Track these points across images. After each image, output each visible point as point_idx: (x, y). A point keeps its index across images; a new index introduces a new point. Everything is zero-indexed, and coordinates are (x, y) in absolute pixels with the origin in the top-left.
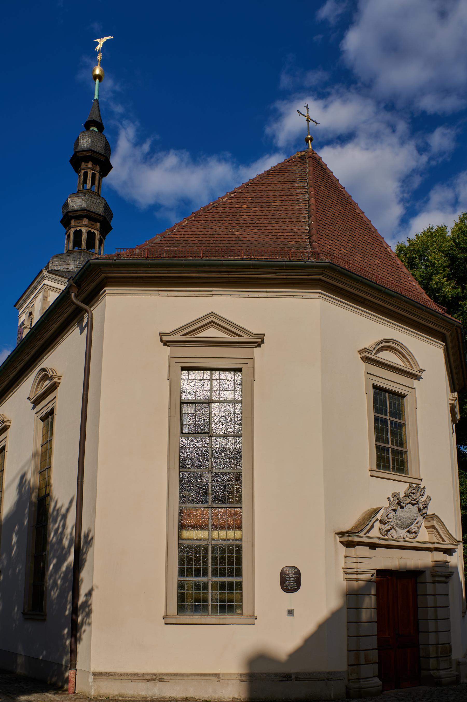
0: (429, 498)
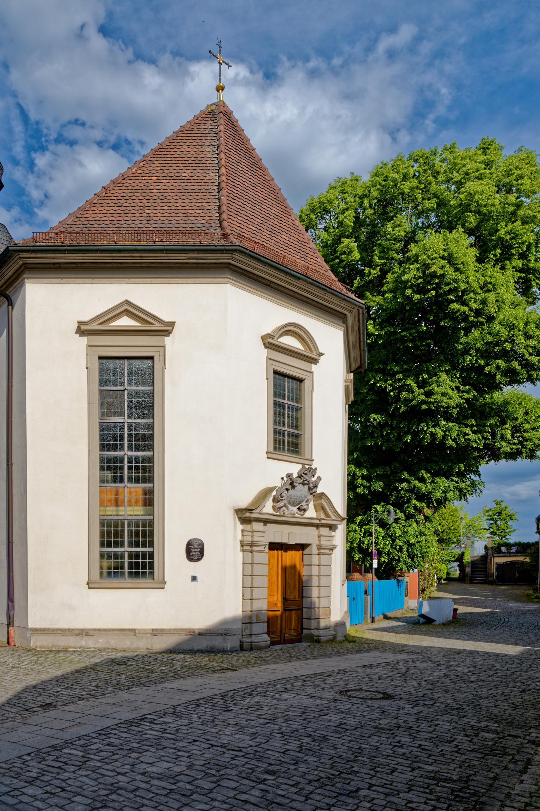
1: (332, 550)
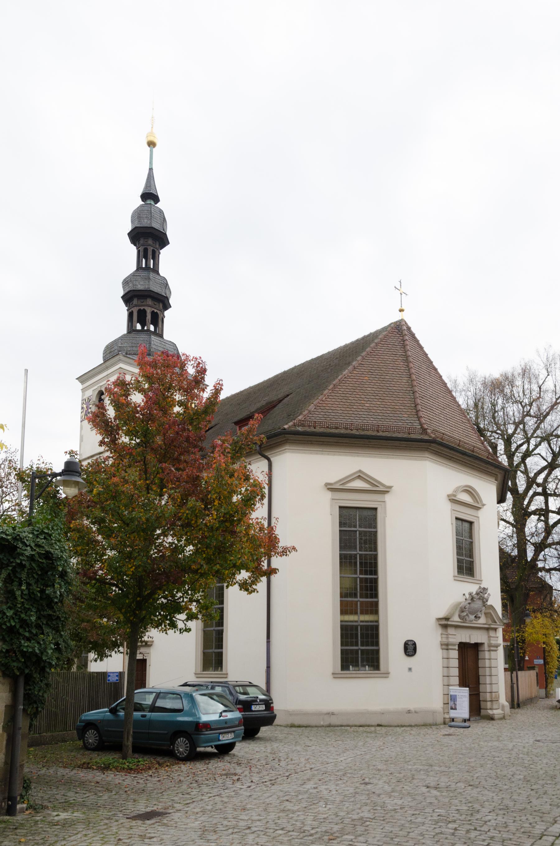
0: (489, 594)
1: (497, 647)
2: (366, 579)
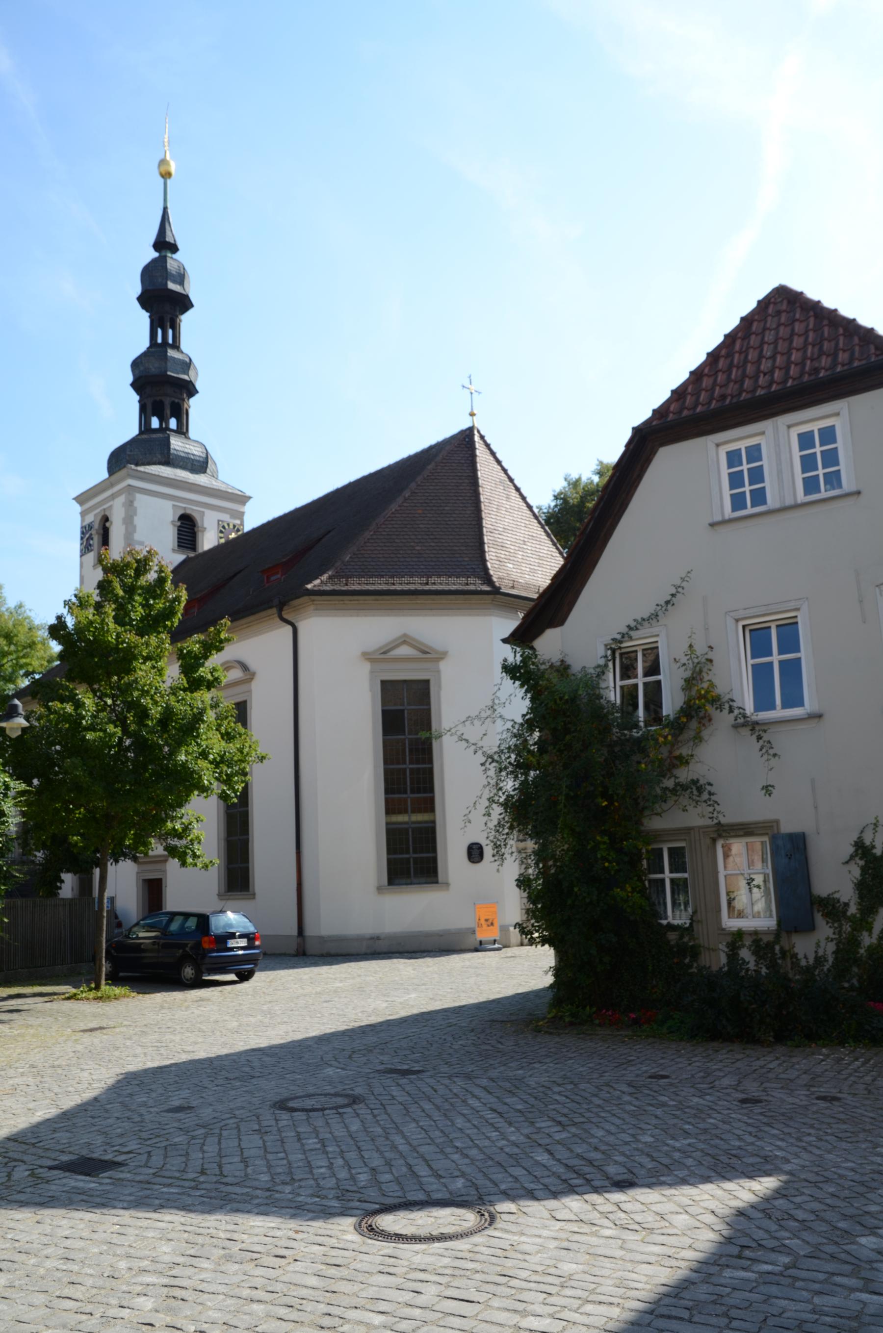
2: (419, 769)
